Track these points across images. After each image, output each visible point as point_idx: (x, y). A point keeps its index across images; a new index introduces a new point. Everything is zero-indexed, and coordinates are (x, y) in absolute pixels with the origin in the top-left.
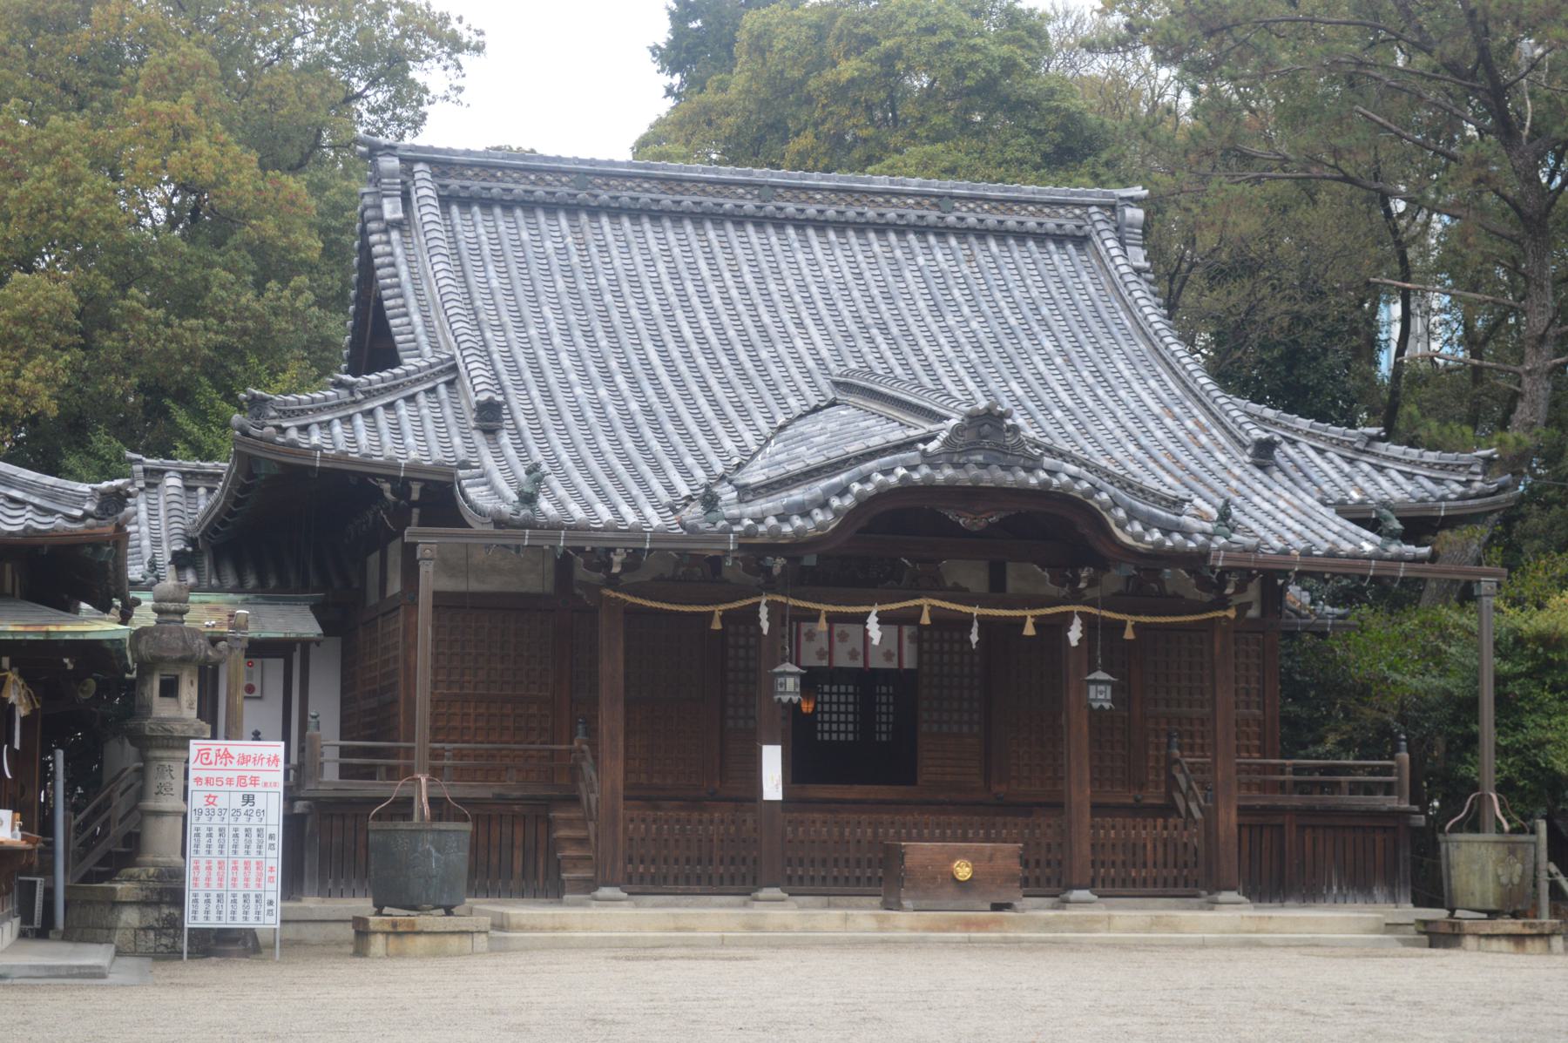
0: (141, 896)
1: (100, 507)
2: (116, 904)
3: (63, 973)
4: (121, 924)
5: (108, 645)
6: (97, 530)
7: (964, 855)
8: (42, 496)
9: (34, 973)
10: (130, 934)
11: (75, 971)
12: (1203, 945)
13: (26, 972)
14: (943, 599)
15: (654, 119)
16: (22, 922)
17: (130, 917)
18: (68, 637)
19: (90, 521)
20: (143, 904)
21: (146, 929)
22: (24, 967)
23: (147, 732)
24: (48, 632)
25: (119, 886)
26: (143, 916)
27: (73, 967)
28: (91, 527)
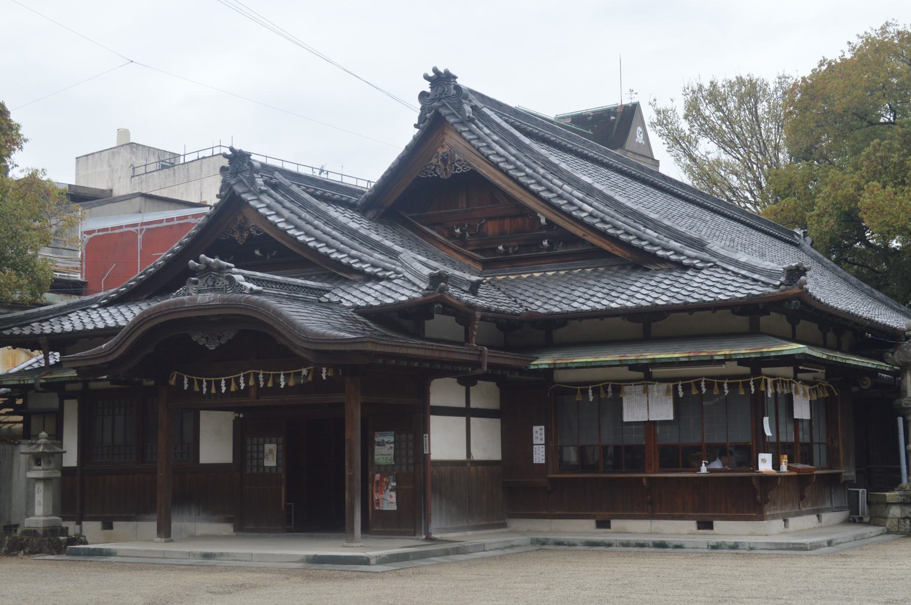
0: (900, 499)
1: (787, 278)
2: (888, 504)
3: (784, 547)
4: (890, 516)
5: (797, 357)
6: (787, 292)
7: (373, 476)
8: (766, 276)
9: (769, 547)
10: (895, 522)
11: (791, 546)
12: (626, 545)
13: (764, 546)
14: (306, 278)
15: (870, 26)
16: (851, 514)
17: (895, 512)
18: (773, 354)
19: (782, 287)
20: (902, 504)
21: (905, 518)
22: (763, 543)
23: (904, 405)
24: (762, 352)
25: (887, 494)
26: (903, 511)
27: (799, 544)
28: (782, 291)
